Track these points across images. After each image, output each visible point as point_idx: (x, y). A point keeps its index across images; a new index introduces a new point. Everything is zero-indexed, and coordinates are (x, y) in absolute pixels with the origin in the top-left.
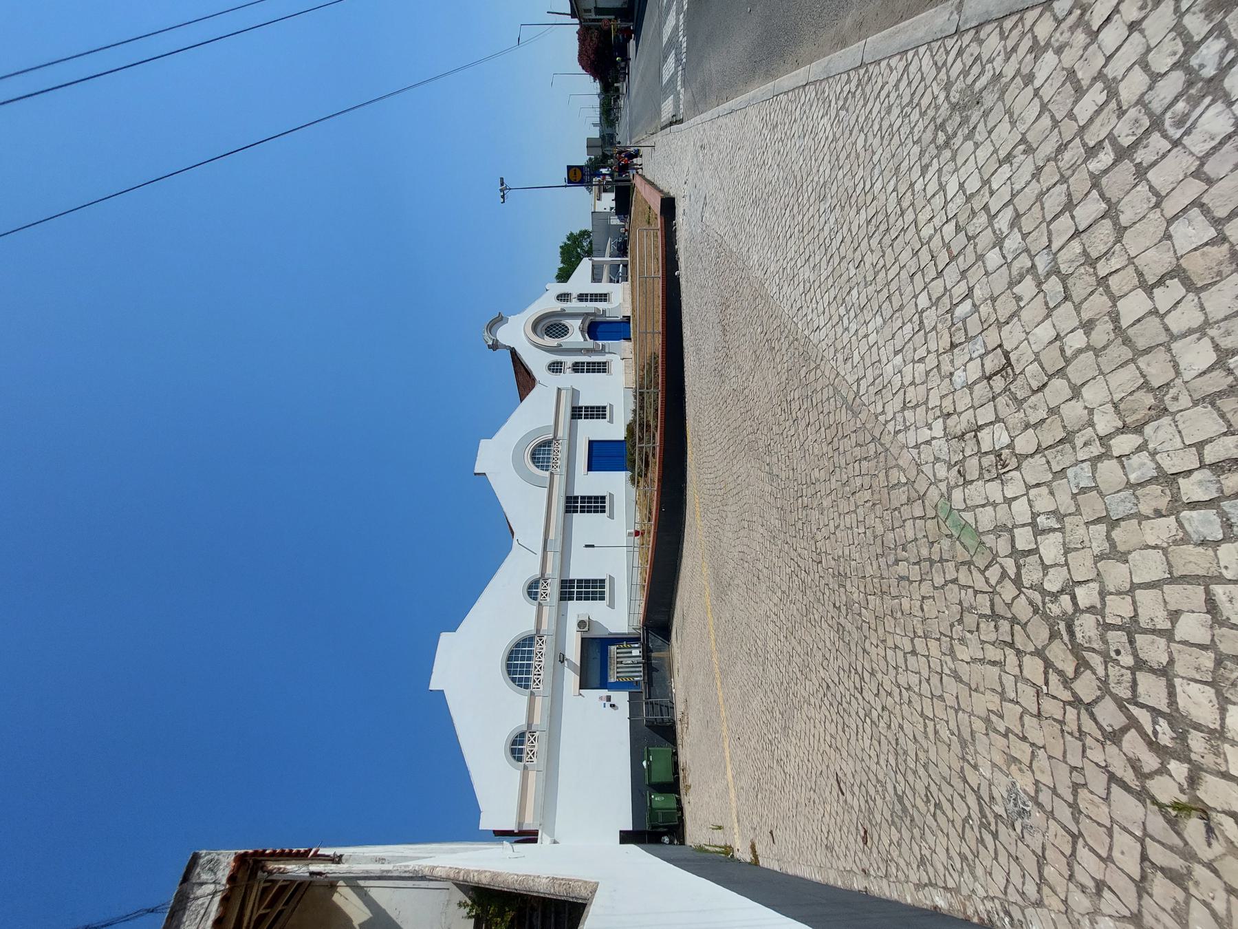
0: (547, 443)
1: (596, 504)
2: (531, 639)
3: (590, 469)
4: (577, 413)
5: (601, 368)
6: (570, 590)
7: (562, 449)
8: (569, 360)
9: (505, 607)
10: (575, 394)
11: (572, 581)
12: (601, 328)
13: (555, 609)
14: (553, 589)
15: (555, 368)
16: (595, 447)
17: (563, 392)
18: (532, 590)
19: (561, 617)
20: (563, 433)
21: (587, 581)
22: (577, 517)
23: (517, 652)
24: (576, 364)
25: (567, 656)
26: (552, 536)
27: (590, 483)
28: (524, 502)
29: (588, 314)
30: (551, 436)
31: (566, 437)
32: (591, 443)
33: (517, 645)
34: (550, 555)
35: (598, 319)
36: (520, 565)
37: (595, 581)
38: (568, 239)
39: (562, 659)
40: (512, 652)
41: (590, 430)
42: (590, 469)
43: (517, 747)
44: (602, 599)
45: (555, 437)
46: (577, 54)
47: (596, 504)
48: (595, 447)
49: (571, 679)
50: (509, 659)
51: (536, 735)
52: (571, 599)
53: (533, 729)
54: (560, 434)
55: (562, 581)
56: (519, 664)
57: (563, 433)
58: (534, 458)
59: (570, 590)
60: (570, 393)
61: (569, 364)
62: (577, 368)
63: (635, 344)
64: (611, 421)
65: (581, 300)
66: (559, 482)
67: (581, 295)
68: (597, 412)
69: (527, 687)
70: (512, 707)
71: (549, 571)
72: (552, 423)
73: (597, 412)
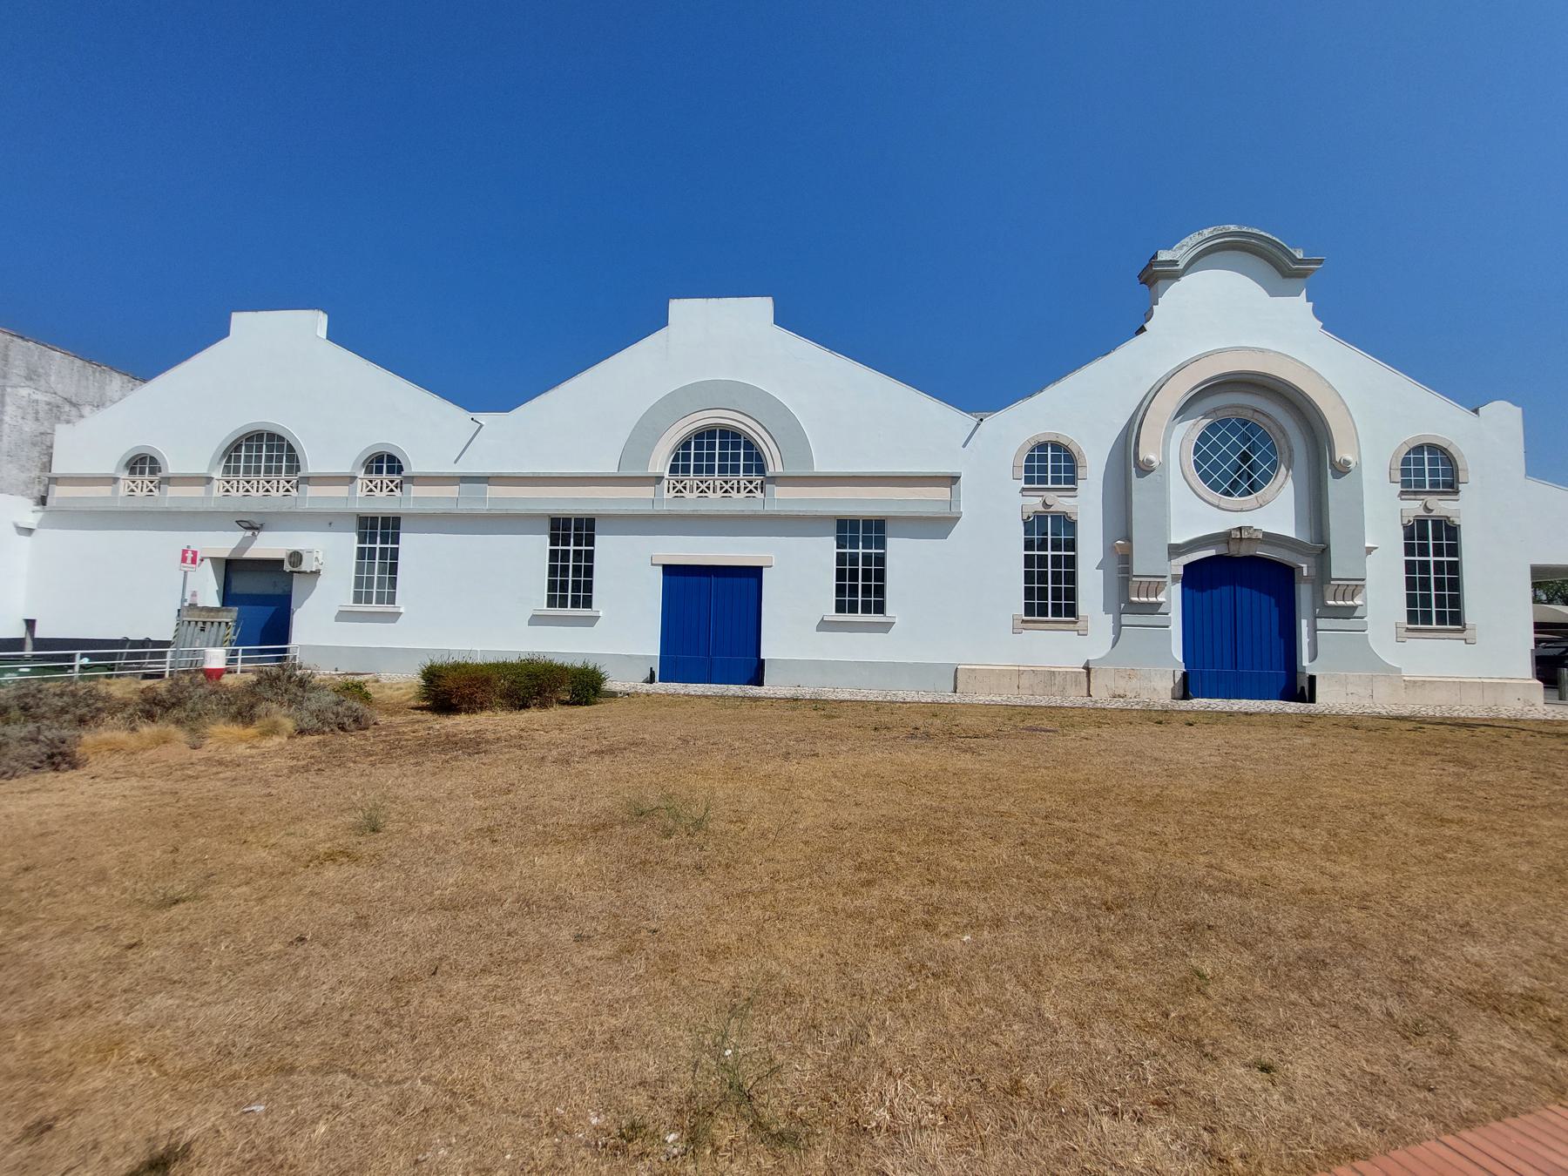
0: (756, 462)
1: (571, 583)
2: (761, 469)
3: (670, 571)
5: (1049, 591)
6: (380, 533)
8: (1086, 504)
9: (846, 416)
10: (938, 525)
11: (881, 543)
12: (1256, 604)
13: (341, 507)
14: (382, 502)
15: (1051, 463)
17: (943, 493)
18: (384, 463)
19: (328, 521)
20: (783, 499)
22: (540, 545)
23: (280, 448)
24: (1067, 524)
25: (262, 535)
26: (493, 491)
28: (594, 422)
29: (1321, 554)
30: (774, 467)
32: (755, 573)
33: (291, 448)
34: (451, 491)
35: (1304, 594)
36: (433, 431)
37: (1456, 601)
39: (254, 528)
40: (281, 438)
42: (670, 571)
43: (142, 463)
44: (840, 608)
46: (552, 393)
47: (571, 583)
49: (225, 543)
50: (271, 436)
51: (758, 494)
52: (362, 540)
53: (768, 487)
56: (263, 450)
57: (783, 499)
58: (704, 436)
59: (380, 533)
61: (1062, 503)
63: (1161, 718)
64: (824, 626)
65: (1415, 534)
66: (637, 499)
67: (1448, 533)
68: (861, 587)
69: (674, 469)
70: (191, 451)
71: (415, 491)
72: (820, 467)
73: (861, 587)
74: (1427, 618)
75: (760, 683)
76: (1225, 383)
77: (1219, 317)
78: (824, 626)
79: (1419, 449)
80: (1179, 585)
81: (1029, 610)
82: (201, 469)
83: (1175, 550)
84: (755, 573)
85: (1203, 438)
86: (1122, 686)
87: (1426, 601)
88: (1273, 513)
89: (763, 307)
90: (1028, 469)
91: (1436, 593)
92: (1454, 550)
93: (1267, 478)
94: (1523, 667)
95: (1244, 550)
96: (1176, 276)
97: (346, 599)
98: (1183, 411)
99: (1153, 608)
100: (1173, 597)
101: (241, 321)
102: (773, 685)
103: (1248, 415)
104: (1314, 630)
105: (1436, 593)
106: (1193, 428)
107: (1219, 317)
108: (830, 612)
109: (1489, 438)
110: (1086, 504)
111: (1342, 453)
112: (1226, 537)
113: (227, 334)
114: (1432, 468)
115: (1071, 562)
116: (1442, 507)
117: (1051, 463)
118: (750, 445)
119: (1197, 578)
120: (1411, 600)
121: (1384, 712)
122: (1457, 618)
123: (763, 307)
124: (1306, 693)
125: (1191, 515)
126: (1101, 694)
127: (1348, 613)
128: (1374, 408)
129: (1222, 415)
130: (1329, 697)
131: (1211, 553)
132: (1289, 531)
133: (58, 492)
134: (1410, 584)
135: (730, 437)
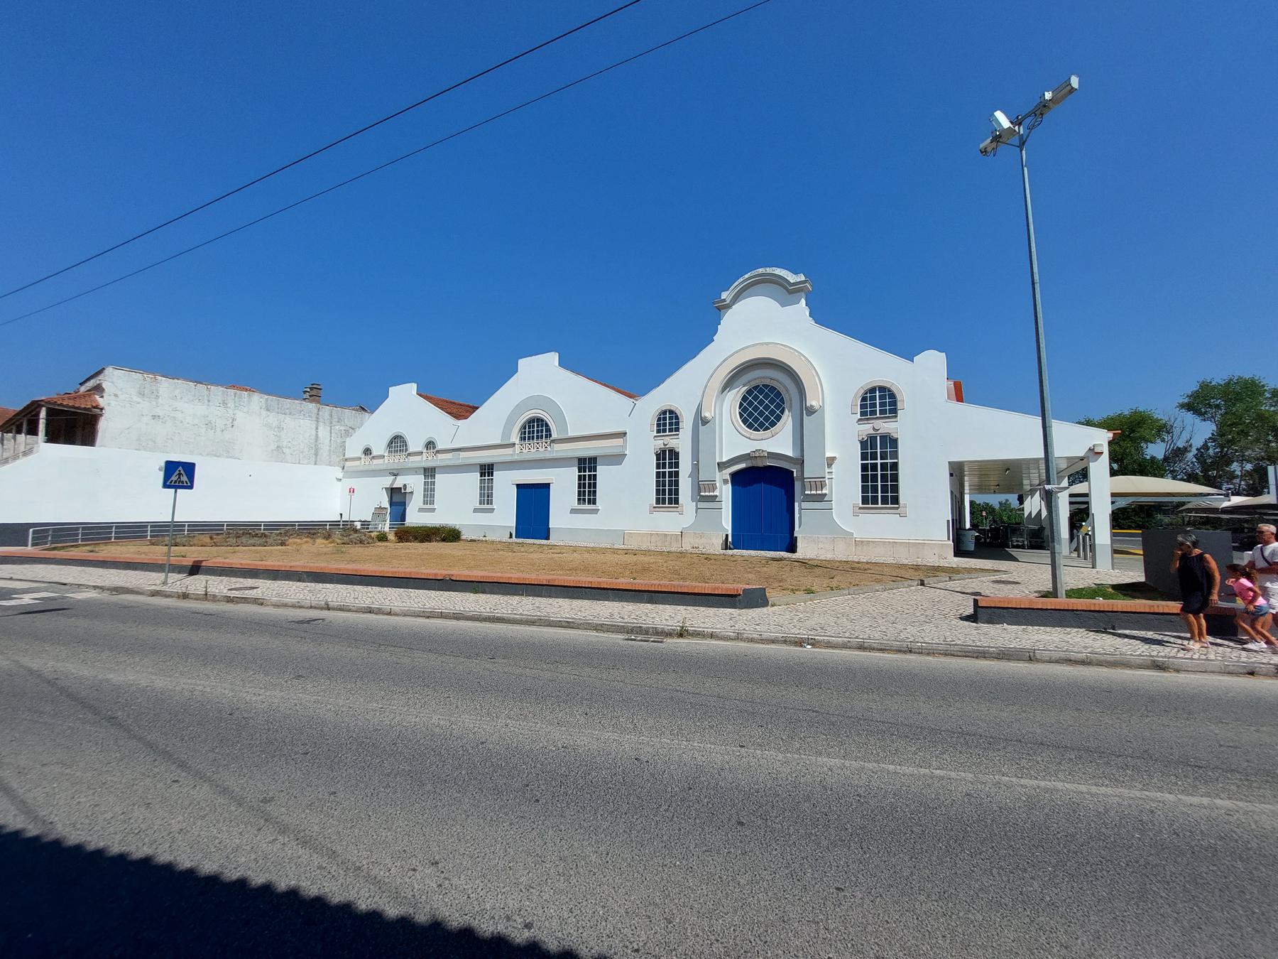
1: (486, 497)
2: (549, 435)
4: (587, 465)
5: (667, 493)
7: (538, 450)
10: (617, 459)
15: (668, 421)
16: (543, 489)
17: (619, 441)
19: (414, 471)
20: (560, 450)
21: (895, 478)
24: (674, 454)
26: (463, 454)
27: (505, 486)
31: (555, 455)
32: (547, 486)
37: (895, 489)
38: (1201, 387)
41: (564, 484)
45: (553, 441)
48: (543, 489)
54: (557, 447)
55: (595, 459)
57: (560, 450)
58: (531, 421)
60: (615, 451)
61: (672, 442)
62: (667, 458)
64: (573, 511)
65: (867, 446)
67: (890, 442)
68: (587, 491)
73: (587, 491)
74: (875, 501)
75: (548, 538)
76: (744, 369)
77: (762, 324)
78: (573, 511)
79: (872, 390)
80: (730, 485)
81: (658, 501)
82: (420, 449)
83: (722, 466)
84: (547, 486)
85: (744, 399)
86: (697, 542)
87: (875, 489)
88: (778, 442)
89: (554, 357)
90: (658, 425)
91: (880, 483)
92: (895, 455)
93: (779, 418)
94: (940, 534)
95: (760, 464)
96: (729, 307)
97: (421, 505)
98: (728, 384)
99: (713, 499)
100: (725, 492)
101: (522, 363)
102: (552, 541)
103: (767, 382)
104: (801, 509)
105: (880, 483)
106: (736, 395)
107: (762, 324)
108: (575, 504)
109: (922, 377)
110: (682, 442)
111: (812, 402)
112: (746, 457)
113: (783, 306)
114: (879, 401)
115: (677, 474)
116: (885, 426)
117: (668, 421)
118: (547, 425)
119: (737, 478)
120: (864, 489)
121: (906, 562)
122: (895, 500)
123: (554, 357)
124: (792, 548)
125: (735, 441)
126: (687, 547)
127: (821, 498)
128: (835, 368)
129: (754, 384)
130: (805, 549)
131: (743, 466)
132: (790, 453)
133: (348, 464)
134: (864, 479)
135: (540, 421)
